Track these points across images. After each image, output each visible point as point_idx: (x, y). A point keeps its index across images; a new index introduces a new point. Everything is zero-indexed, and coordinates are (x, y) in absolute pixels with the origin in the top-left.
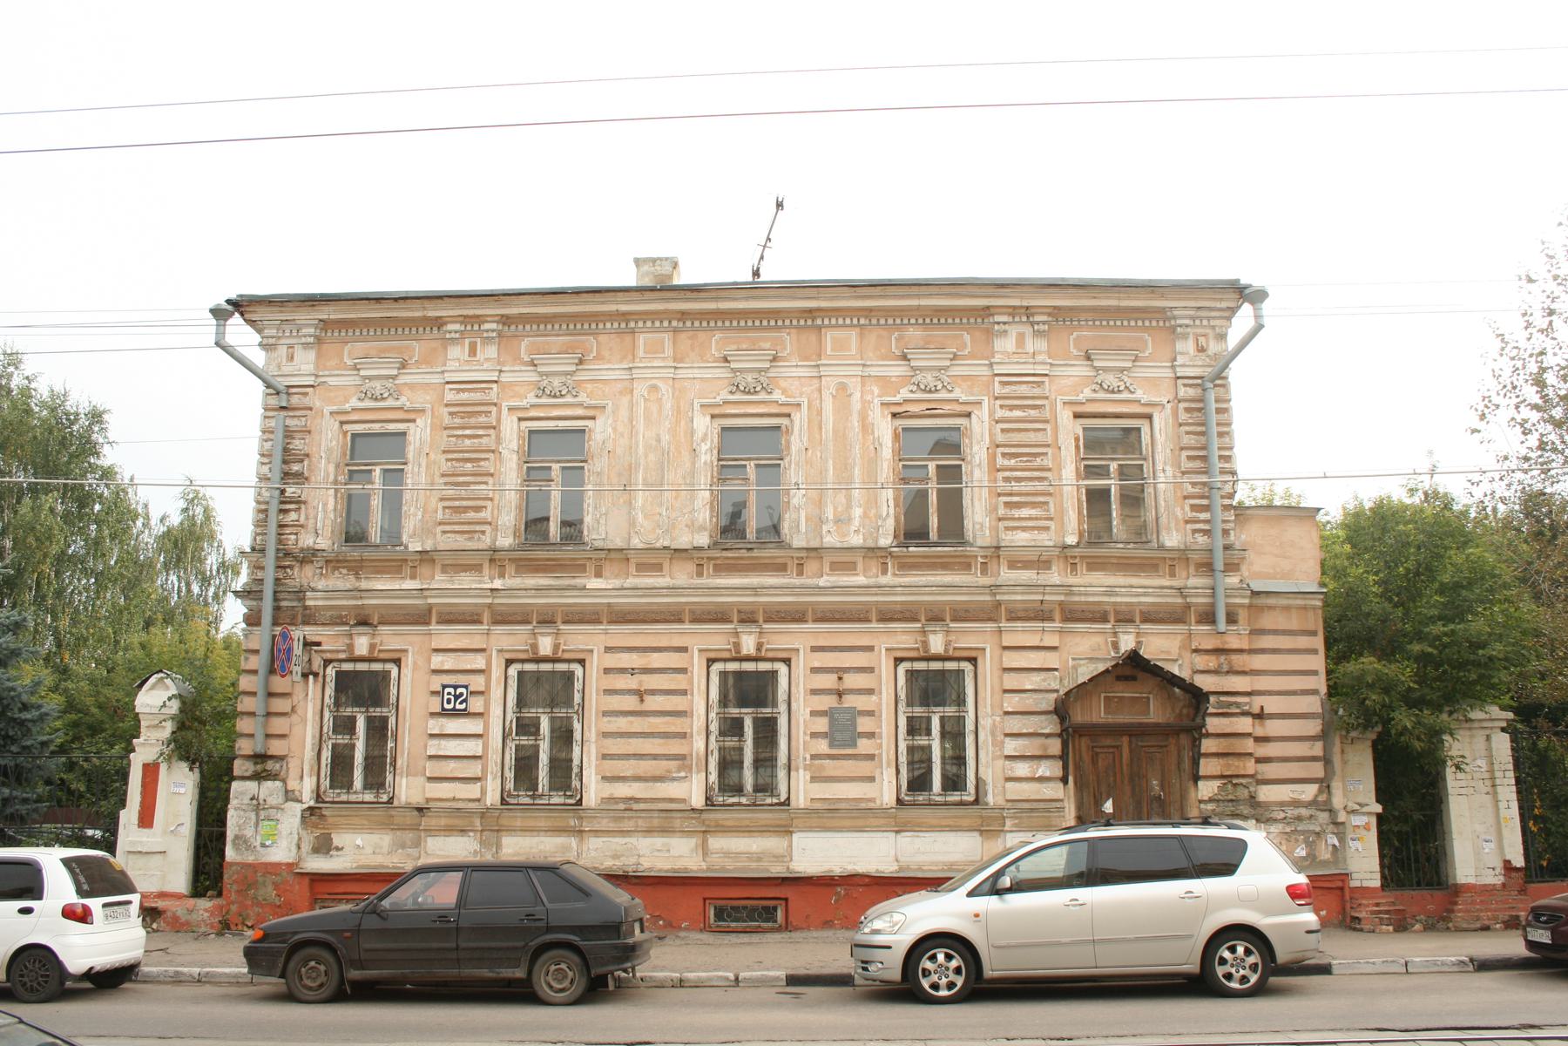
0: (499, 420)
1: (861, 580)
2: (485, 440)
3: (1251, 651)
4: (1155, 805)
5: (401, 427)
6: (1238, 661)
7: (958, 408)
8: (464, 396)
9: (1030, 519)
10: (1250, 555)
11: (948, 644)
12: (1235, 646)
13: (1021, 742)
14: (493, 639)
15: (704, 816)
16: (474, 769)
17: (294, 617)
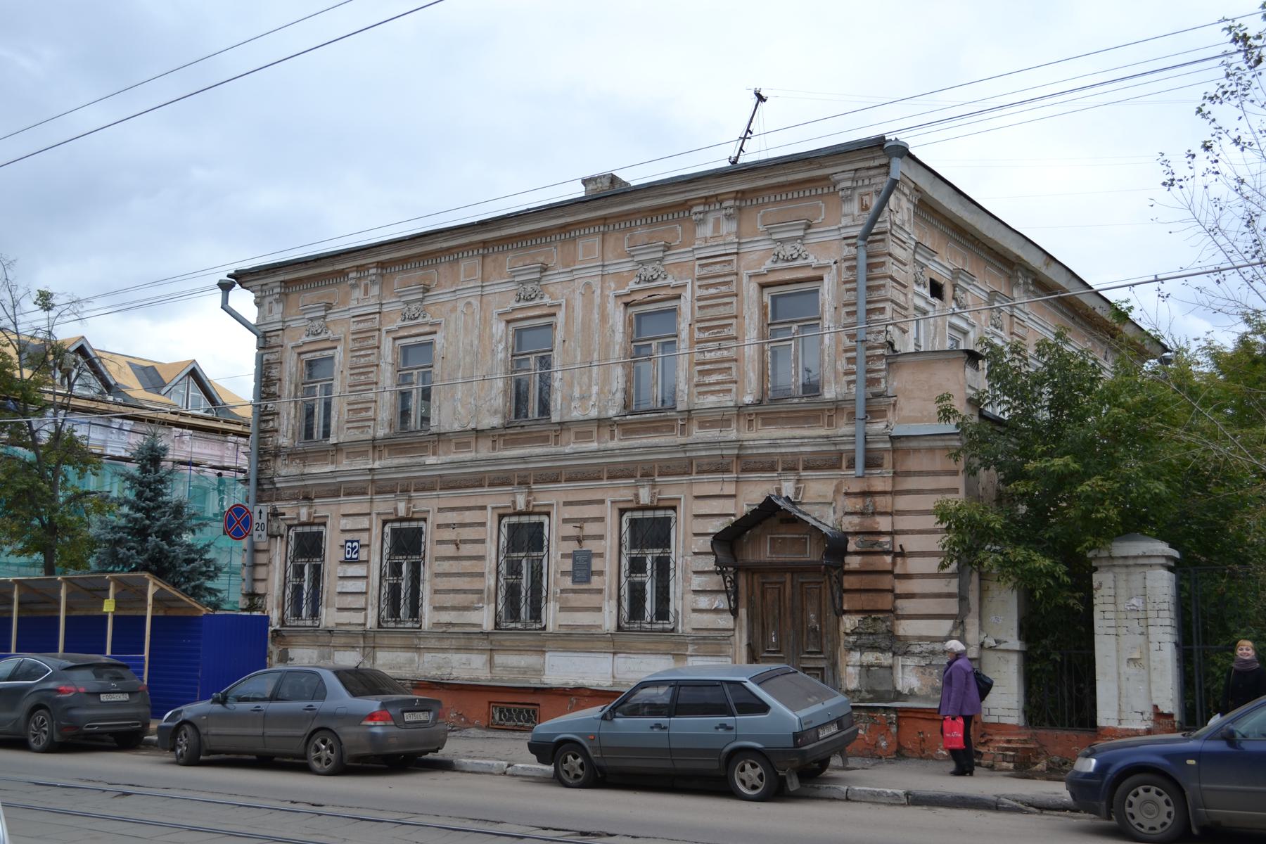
0: (380, 341)
1: (594, 446)
2: (372, 358)
3: (894, 493)
4: (812, 636)
5: (331, 352)
6: (883, 502)
7: (670, 292)
8: (362, 326)
9: (718, 383)
10: (902, 402)
11: (653, 495)
12: (879, 488)
13: (704, 578)
14: (375, 505)
15: (491, 637)
16: (360, 602)
17: (271, 496)
